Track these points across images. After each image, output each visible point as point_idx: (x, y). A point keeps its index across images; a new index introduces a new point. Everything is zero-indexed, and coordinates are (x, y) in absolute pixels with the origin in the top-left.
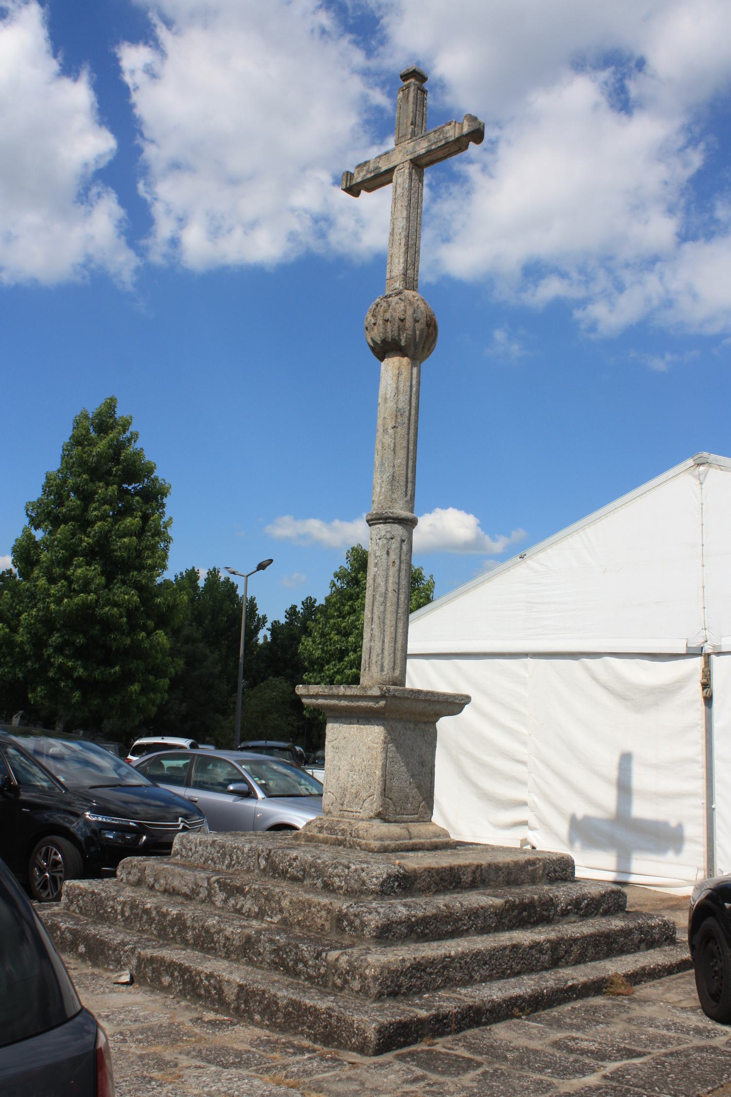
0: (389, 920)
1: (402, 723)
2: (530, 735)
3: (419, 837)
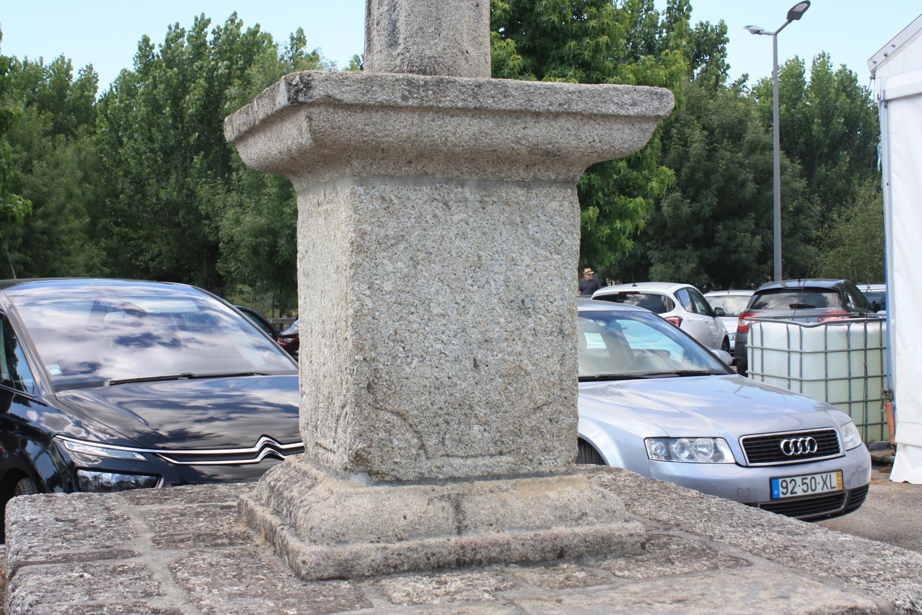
1: (426, 189)
3: (499, 524)
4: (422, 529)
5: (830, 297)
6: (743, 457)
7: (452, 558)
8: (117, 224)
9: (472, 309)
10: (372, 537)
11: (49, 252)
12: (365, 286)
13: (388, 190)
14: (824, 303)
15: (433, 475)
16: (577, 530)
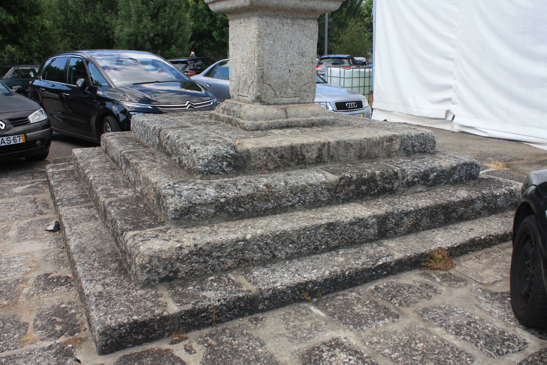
0: (191, 202)
1: (278, 20)
2: (458, 40)
3: (297, 116)
4: (277, 117)
5: (345, 61)
6: (335, 109)
7: (285, 125)
8: (69, 32)
9: (289, 55)
10: (264, 119)
11: (48, 42)
12: (261, 48)
13: (267, 19)
14: (343, 63)
15: (278, 103)
16: (317, 118)
